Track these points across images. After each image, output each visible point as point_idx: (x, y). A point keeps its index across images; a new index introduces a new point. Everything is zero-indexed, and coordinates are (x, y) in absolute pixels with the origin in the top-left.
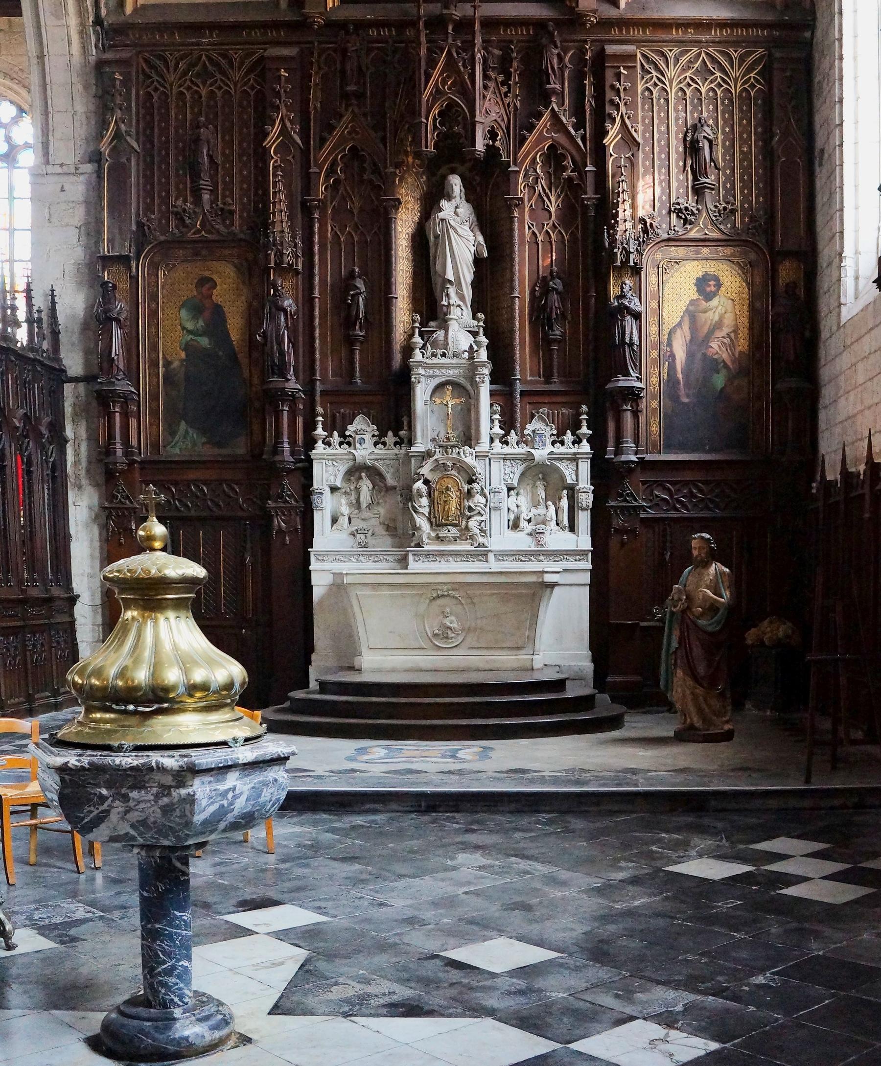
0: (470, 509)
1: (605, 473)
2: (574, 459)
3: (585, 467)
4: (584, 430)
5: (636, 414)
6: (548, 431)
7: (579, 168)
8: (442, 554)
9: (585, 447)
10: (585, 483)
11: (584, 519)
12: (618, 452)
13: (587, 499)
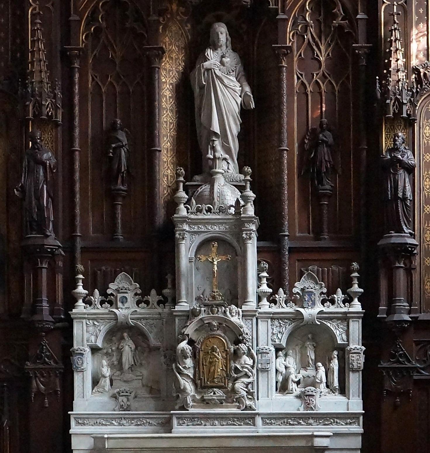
0: (237, 370)
1: (376, 332)
2: (345, 318)
3: (356, 327)
4: (356, 288)
5: (409, 271)
6: (318, 290)
7: (349, 16)
8: (207, 418)
9: (357, 306)
10: (356, 344)
11: (355, 381)
12: (391, 311)
13: (358, 360)
